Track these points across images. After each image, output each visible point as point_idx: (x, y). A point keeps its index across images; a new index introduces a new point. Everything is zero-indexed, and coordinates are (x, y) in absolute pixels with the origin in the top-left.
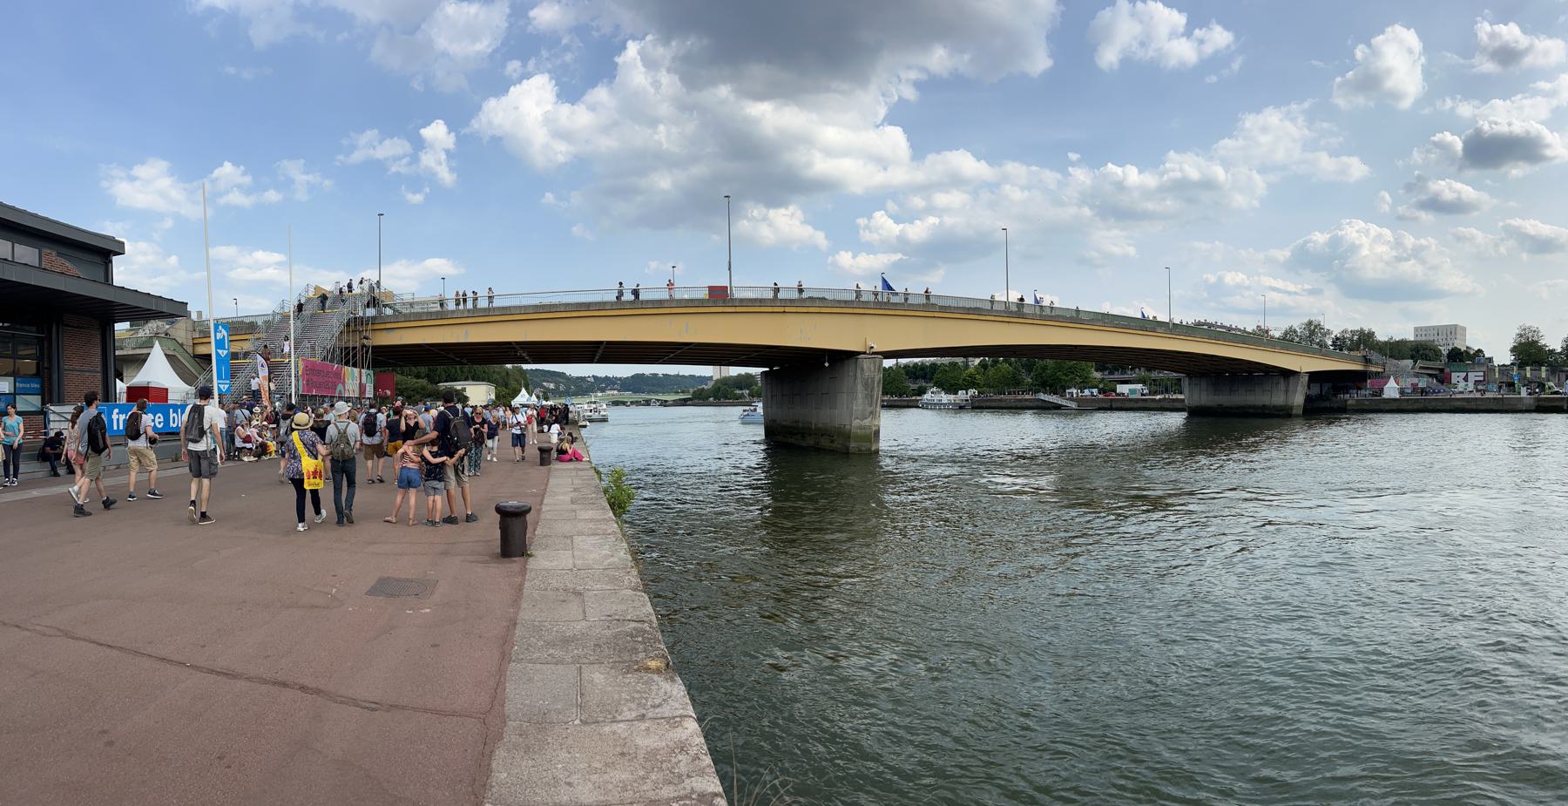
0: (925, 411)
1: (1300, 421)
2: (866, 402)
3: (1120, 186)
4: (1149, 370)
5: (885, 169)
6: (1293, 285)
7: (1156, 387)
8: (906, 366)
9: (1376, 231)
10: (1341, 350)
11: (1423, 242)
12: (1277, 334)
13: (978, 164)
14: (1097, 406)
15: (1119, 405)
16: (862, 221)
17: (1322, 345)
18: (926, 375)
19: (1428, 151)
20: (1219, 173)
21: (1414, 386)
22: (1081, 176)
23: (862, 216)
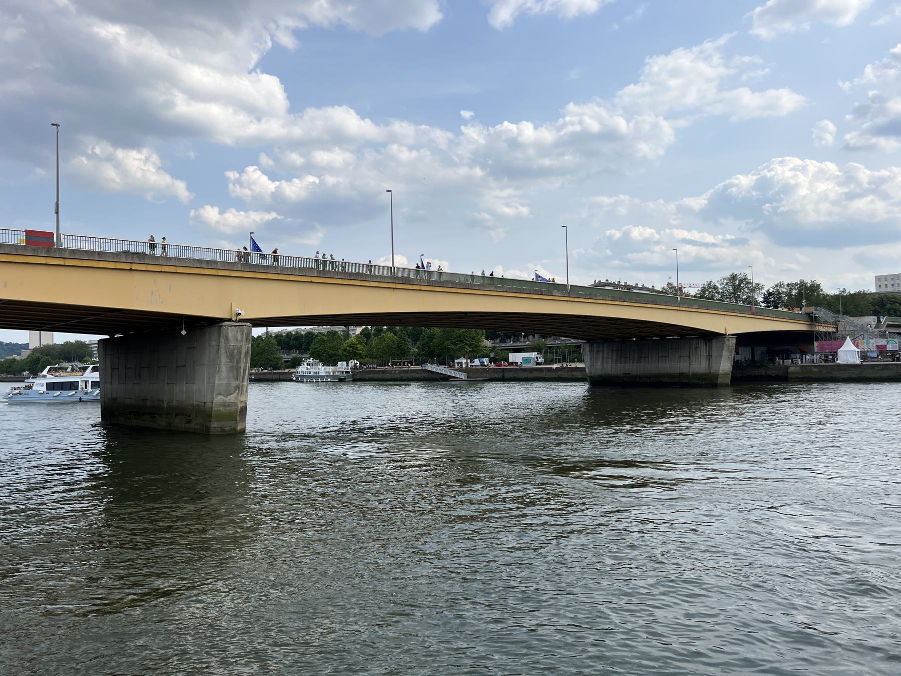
0: (300, 385)
1: (728, 391)
2: (231, 375)
3: (514, 143)
4: (544, 336)
5: (259, 120)
6: (712, 236)
7: (551, 354)
8: (278, 336)
9: (815, 166)
10: (776, 307)
11: (884, 173)
12: (693, 292)
13: (362, 123)
14: (488, 376)
15: (511, 375)
16: (232, 175)
17: (750, 301)
18: (301, 345)
19: (888, 66)
20: (622, 124)
21: (882, 350)
22: (475, 135)
23: (232, 170)
